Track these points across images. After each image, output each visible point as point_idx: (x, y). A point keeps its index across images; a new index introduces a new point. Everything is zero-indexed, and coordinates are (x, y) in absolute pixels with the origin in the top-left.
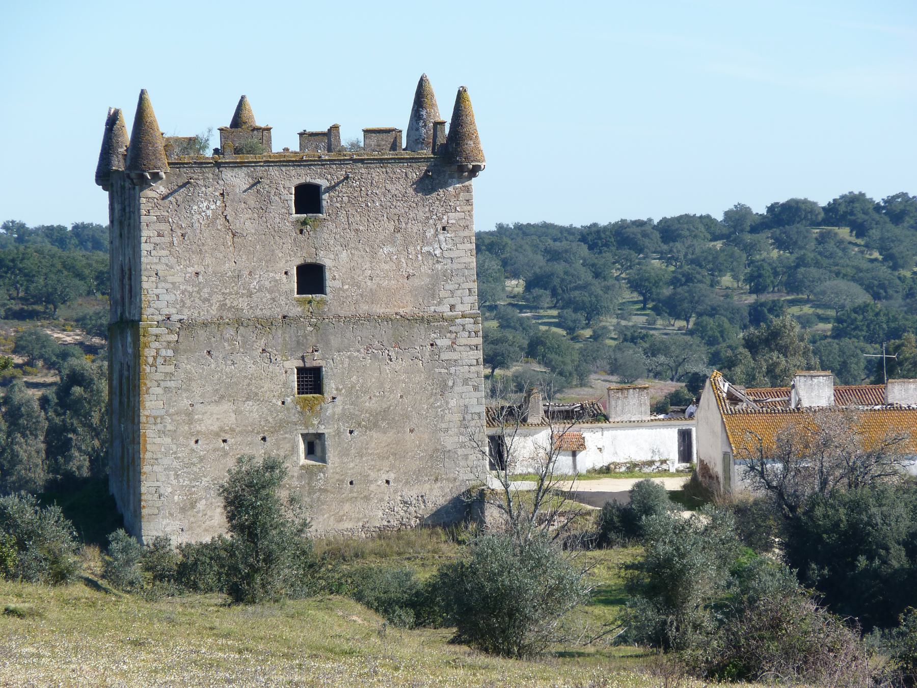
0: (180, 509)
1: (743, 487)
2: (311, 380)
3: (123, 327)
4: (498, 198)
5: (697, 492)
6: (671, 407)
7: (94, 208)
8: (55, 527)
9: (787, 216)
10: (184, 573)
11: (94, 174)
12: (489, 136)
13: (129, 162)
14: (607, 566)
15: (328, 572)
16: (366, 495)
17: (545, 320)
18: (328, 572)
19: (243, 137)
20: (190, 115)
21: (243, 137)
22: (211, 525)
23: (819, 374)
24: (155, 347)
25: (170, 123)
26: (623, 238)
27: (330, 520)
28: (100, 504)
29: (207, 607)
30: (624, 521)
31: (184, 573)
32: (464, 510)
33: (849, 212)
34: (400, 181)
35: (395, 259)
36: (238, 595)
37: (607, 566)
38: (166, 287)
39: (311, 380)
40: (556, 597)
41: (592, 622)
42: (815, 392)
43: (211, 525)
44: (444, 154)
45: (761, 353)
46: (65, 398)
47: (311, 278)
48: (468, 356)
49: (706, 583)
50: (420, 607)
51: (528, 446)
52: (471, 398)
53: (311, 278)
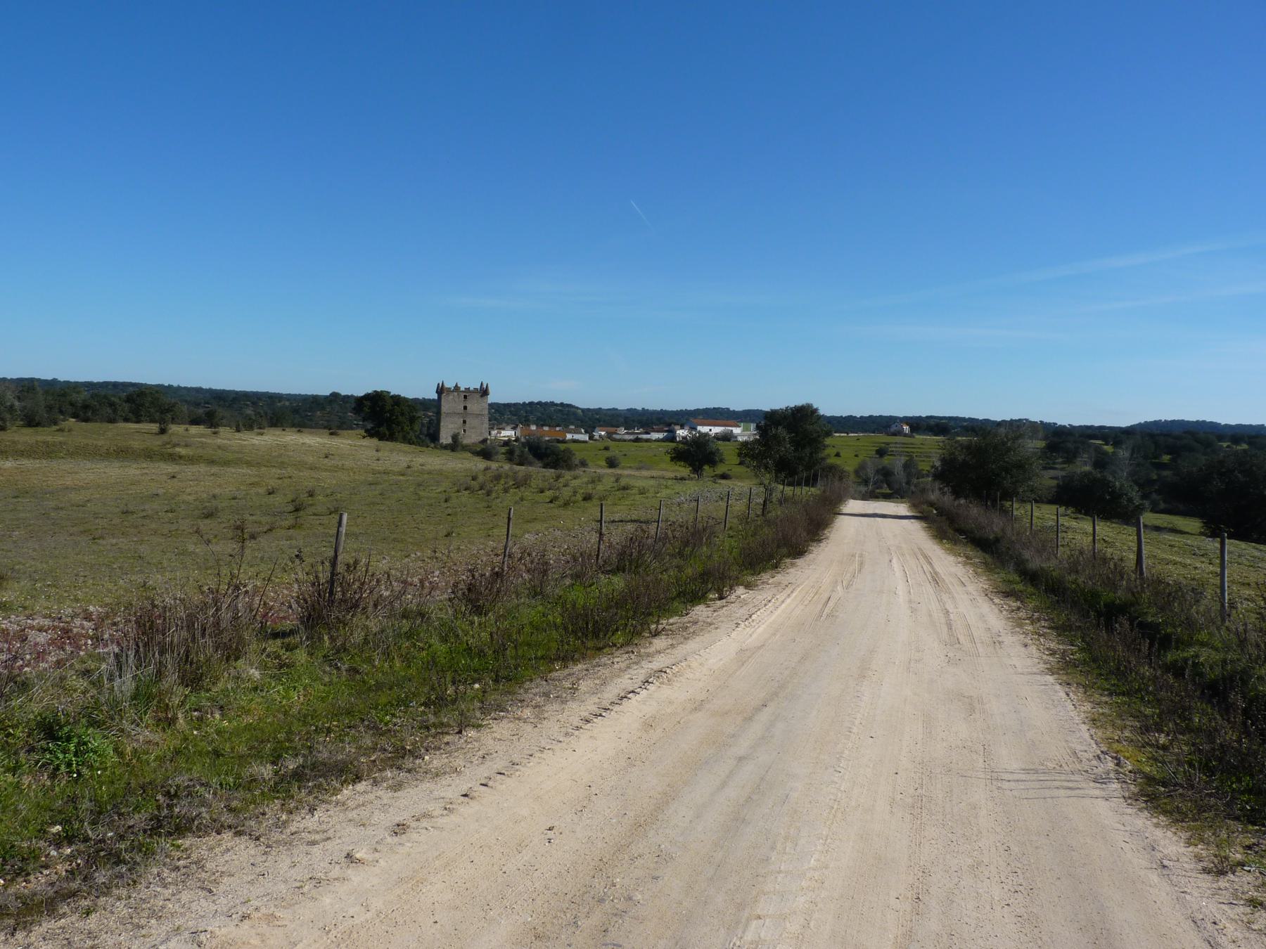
0: (445, 438)
1: (523, 440)
2: (464, 422)
3: (438, 413)
4: (492, 398)
5: (516, 440)
6: (514, 428)
7: (435, 396)
8: (428, 441)
9: (531, 404)
10: (445, 447)
11: (1157, 419)
12: (491, 390)
13: (441, 390)
14: (503, 450)
15: (465, 448)
16: (471, 438)
17: (497, 415)
18: (465, 448)
19: (457, 388)
20: (450, 384)
21: (457, 388)
22: (450, 441)
23: (625, 682)
24: (443, 416)
25: (446, 385)
26: (508, 405)
27: (465, 442)
28: (434, 437)
29: (448, 452)
30: (507, 443)
31: (445, 447)
32: (485, 441)
33: (540, 403)
34: (478, 396)
35: (475, 406)
36: (453, 450)
37: (503, 450)
38: (445, 407)
39: (464, 422)
40: (497, 453)
41: (501, 457)
42: (533, 428)
43: (450, 441)
44: (484, 392)
45: (527, 422)
46: (430, 422)
47: (465, 408)
48: (486, 420)
49: (517, 453)
50: (478, 454)
51: (494, 432)
52: (486, 425)
53: (465, 408)
